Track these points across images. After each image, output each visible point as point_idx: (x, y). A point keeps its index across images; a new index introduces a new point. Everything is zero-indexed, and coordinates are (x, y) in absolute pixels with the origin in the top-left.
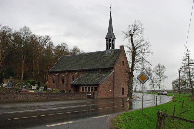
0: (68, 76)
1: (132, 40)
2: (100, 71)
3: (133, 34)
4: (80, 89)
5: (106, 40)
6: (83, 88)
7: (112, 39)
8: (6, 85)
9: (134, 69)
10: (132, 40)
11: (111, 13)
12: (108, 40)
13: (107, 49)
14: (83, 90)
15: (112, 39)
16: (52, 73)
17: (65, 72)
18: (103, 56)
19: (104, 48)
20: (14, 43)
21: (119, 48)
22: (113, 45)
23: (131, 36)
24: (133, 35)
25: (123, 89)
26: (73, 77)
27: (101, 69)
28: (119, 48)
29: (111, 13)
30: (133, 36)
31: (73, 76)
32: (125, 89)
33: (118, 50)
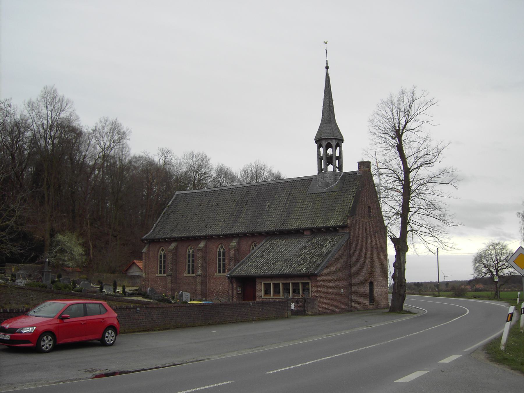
0: (205, 251)
1: (400, 148)
2: (307, 233)
3: (403, 130)
4: (258, 290)
5: (316, 146)
6: (267, 286)
7: (334, 141)
8: (251, 268)
9: (409, 228)
10: (400, 148)
11: (327, 68)
12: (324, 143)
13: (320, 170)
14: (267, 292)
15: (334, 143)
16: (152, 241)
17: (197, 239)
18: (309, 191)
19: (314, 172)
20: (407, 174)
21: (355, 168)
22: (339, 158)
23: (398, 134)
24: (403, 133)
25: (371, 283)
26: (193, 256)
27: (310, 230)
28: (355, 168)
29: (327, 68)
30: (404, 137)
31: (222, 250)
32: (375, 284)
33: (353, 174)
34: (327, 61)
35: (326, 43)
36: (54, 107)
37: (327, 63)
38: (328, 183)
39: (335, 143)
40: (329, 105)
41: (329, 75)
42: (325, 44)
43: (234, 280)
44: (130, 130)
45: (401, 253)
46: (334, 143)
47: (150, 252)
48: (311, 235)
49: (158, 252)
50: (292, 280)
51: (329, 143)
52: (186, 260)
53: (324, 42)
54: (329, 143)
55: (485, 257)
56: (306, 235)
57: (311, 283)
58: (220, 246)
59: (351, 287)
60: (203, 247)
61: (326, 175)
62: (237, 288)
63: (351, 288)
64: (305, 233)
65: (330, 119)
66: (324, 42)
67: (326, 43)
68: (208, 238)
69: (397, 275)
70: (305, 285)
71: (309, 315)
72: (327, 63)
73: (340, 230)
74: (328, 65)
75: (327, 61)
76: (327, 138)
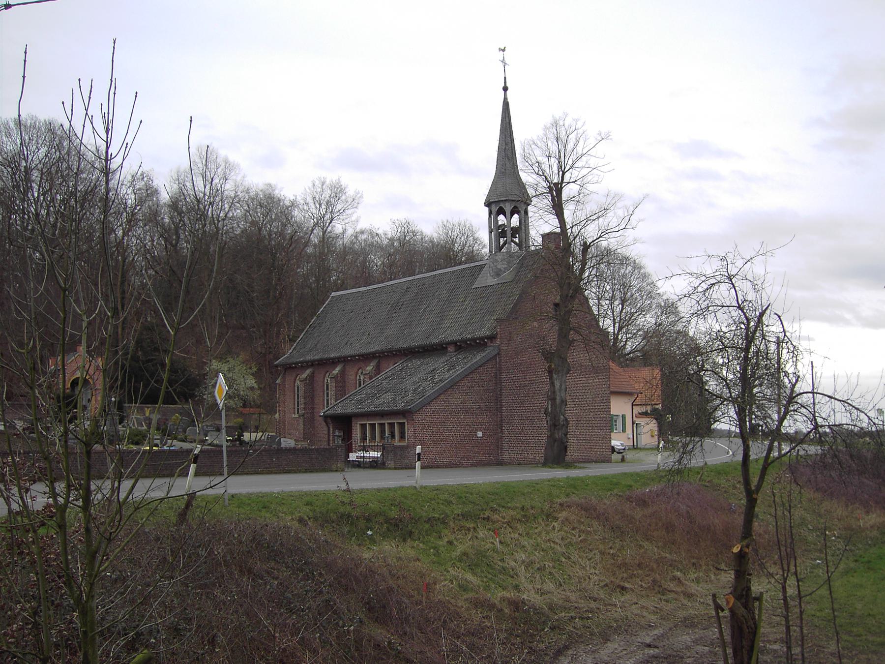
11: (505, 89)
17: (334, 362)
29: (505, 89)
34: (505, 78)
35: (504, 50)
36: (204, 177)
37: (505, 82)
38: (500, 270)
39: (511, 207)
40: (505, 148)
41: (509, 100)
42: (501, 52)
43: (329, 421)
44: (361, 193)
45: (554, 375)
46: (508, 208)
47: (286, 383)
48: (455, 352)
49: (295, 383)
50: (368, 420)
51: (515, 207)
52: (324, 393)
53: (500, 50)
54: (501, 209)
55: (206, 387)
56: (450, 352)
57: (408, 422)
58: (360, 371)
59: (501, 428)
60: (337, 374)
61: (497, 258)
62: (334, 432)
63: (502, 430)
64: (449, 349)
65: (505, 170)
66: (500, 50)
67: (504, 50)
68: (344, 360)
69: (550, 410)
70: (402, 425)
71: (390, 469)
72: (505, 82)
73: (489, 344)
74: (507, 85)
75: (505, 78)
76: (497, 200)
